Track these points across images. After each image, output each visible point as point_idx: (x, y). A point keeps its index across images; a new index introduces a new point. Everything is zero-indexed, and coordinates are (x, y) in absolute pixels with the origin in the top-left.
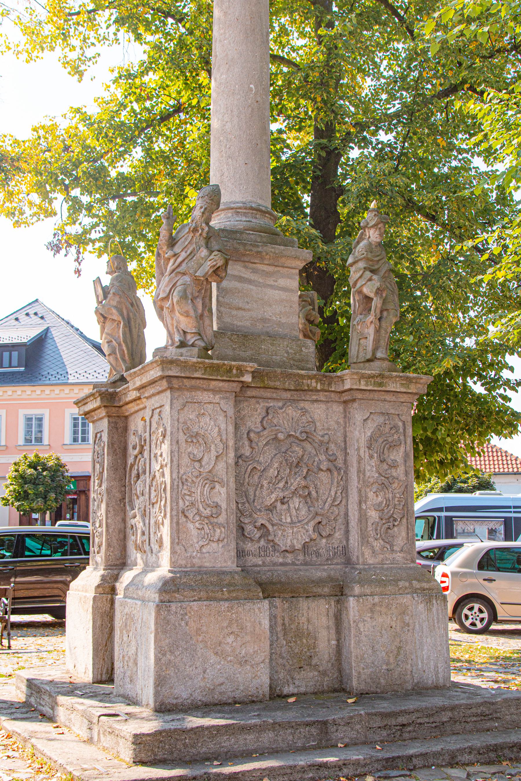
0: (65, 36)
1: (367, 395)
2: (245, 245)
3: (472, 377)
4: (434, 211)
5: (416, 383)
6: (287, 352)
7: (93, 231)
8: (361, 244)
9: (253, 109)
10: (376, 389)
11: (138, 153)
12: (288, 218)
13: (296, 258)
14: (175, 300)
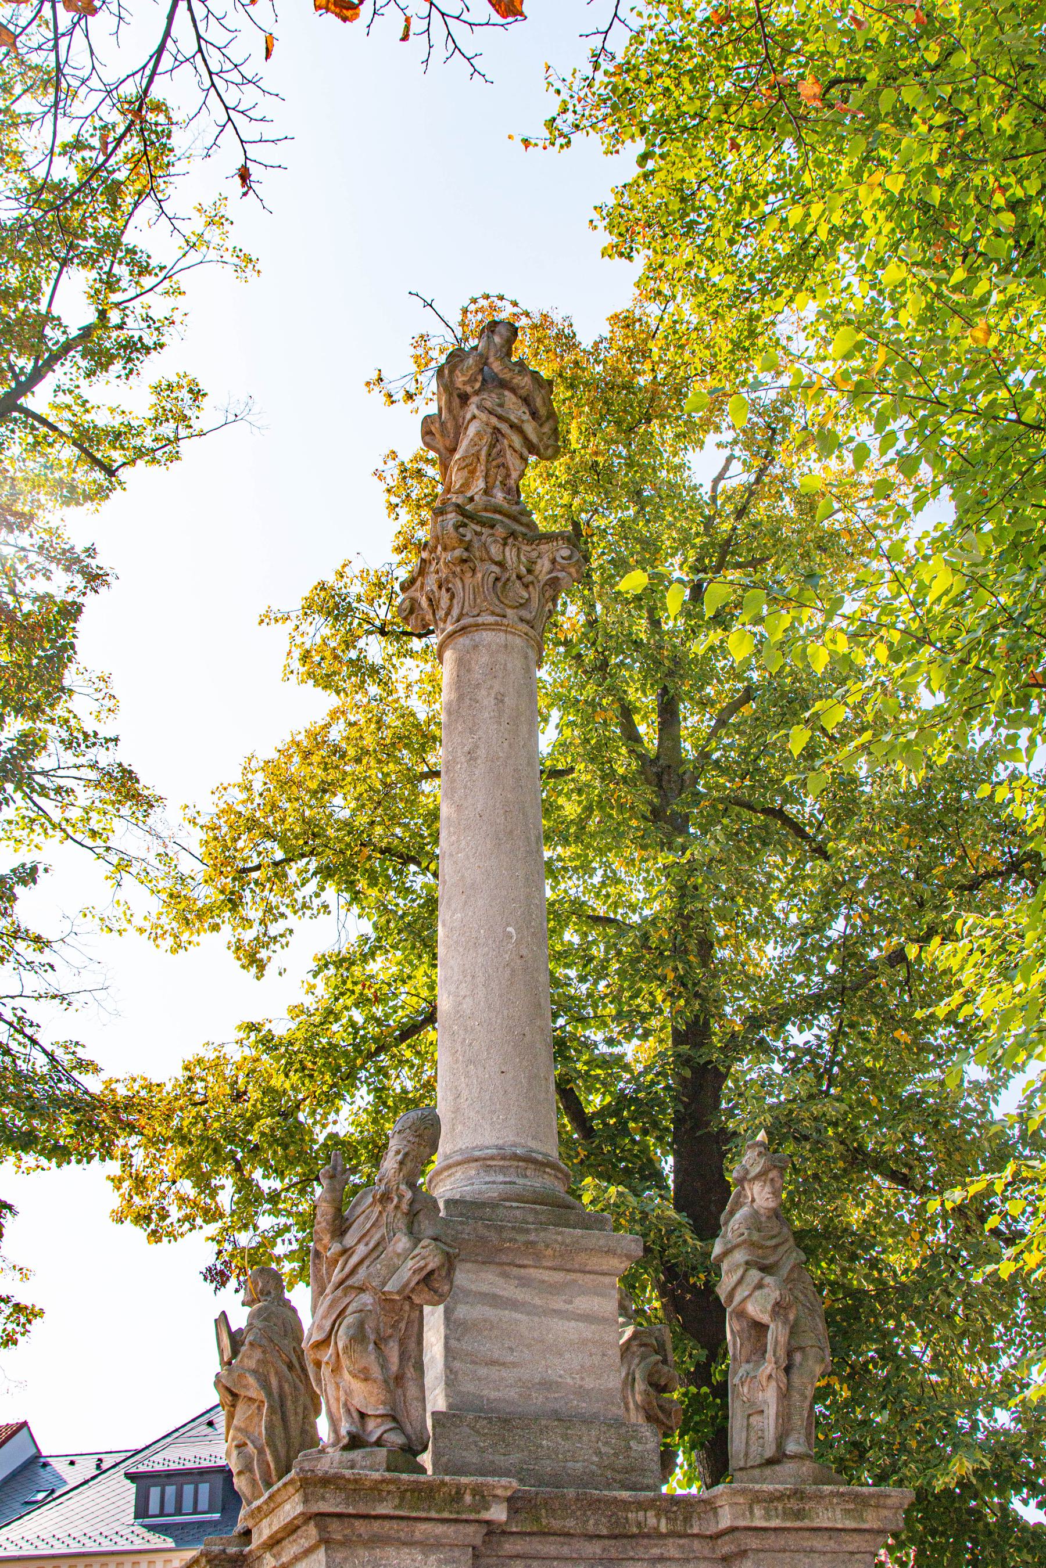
0: (234, 902)
1: (771, 1541)
2: (500, 1229)
3: (1018, 1491)
4: (906, 1165)
5: (877, 1506)
6: (598, 1453)
7: (279, 1240)
8: (737, 1216)
9: (513, 971)
10: (788, 1524)
11: (363, 1097)
12: (621, 1188)
13: (610, 1252)
14: (340, 1345)
